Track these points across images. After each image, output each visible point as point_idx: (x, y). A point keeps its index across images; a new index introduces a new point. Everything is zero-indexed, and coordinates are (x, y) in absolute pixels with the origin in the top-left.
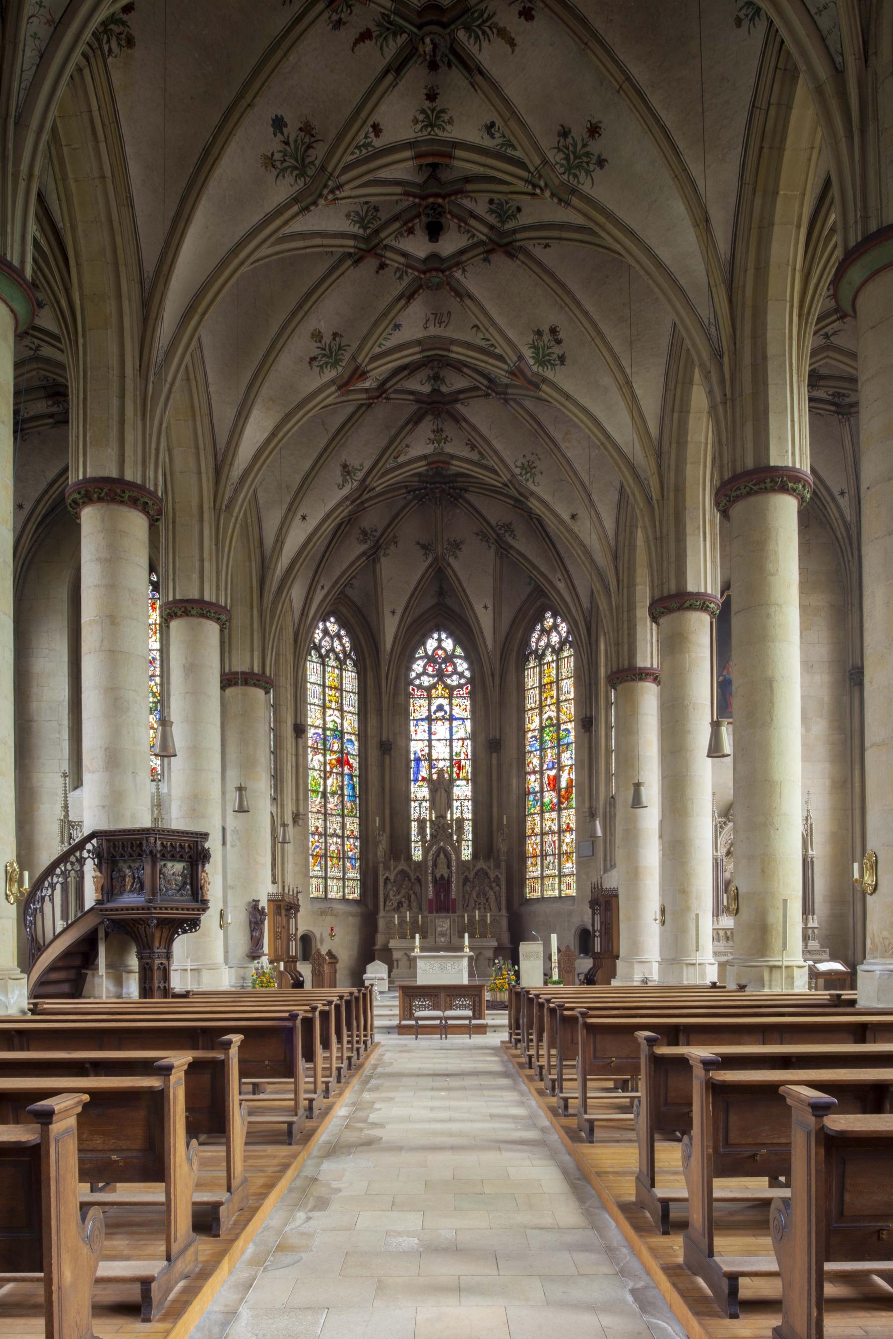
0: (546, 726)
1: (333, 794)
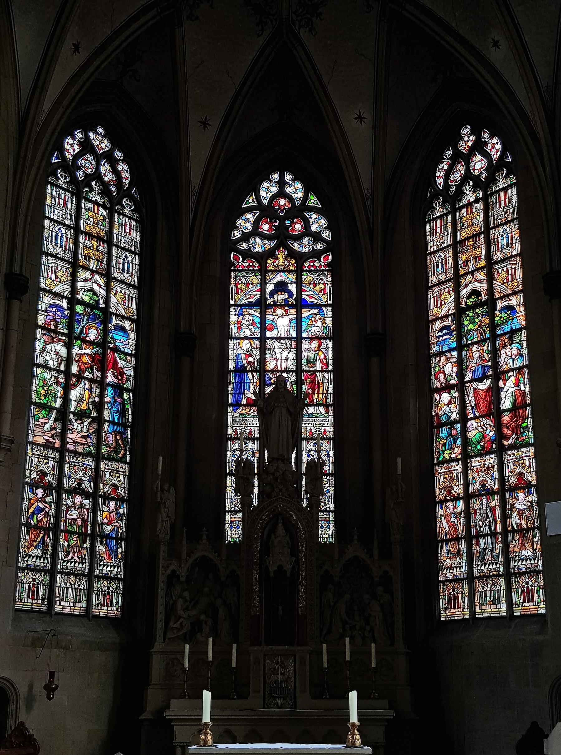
0: (469, 308)
1: (81, 415)
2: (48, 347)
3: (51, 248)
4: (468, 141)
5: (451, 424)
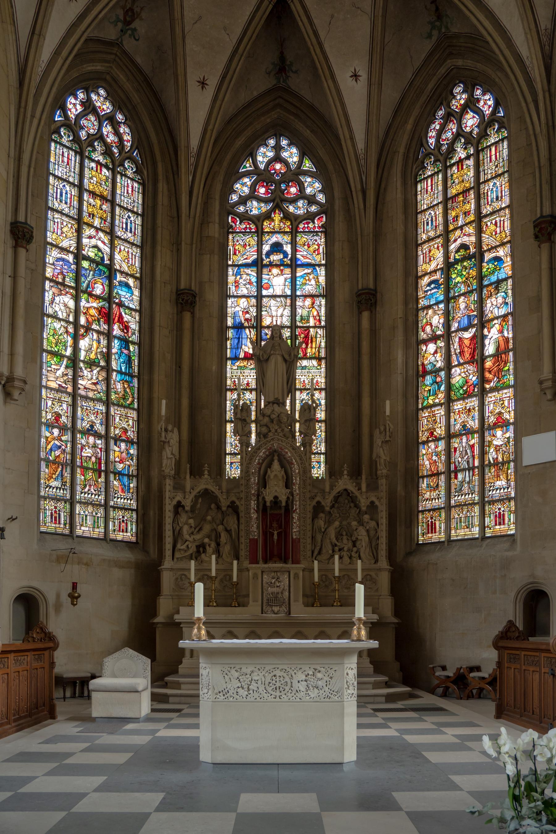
0: (457, 262)
1: (91, 364)
2: (57, 299)
3: (56, 205)
4: (460, 99)
5: (436, 372)
